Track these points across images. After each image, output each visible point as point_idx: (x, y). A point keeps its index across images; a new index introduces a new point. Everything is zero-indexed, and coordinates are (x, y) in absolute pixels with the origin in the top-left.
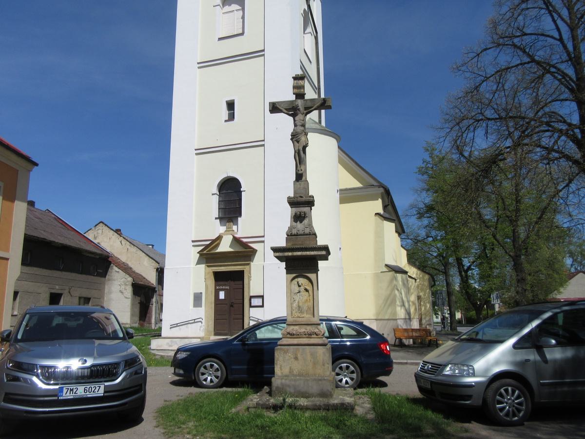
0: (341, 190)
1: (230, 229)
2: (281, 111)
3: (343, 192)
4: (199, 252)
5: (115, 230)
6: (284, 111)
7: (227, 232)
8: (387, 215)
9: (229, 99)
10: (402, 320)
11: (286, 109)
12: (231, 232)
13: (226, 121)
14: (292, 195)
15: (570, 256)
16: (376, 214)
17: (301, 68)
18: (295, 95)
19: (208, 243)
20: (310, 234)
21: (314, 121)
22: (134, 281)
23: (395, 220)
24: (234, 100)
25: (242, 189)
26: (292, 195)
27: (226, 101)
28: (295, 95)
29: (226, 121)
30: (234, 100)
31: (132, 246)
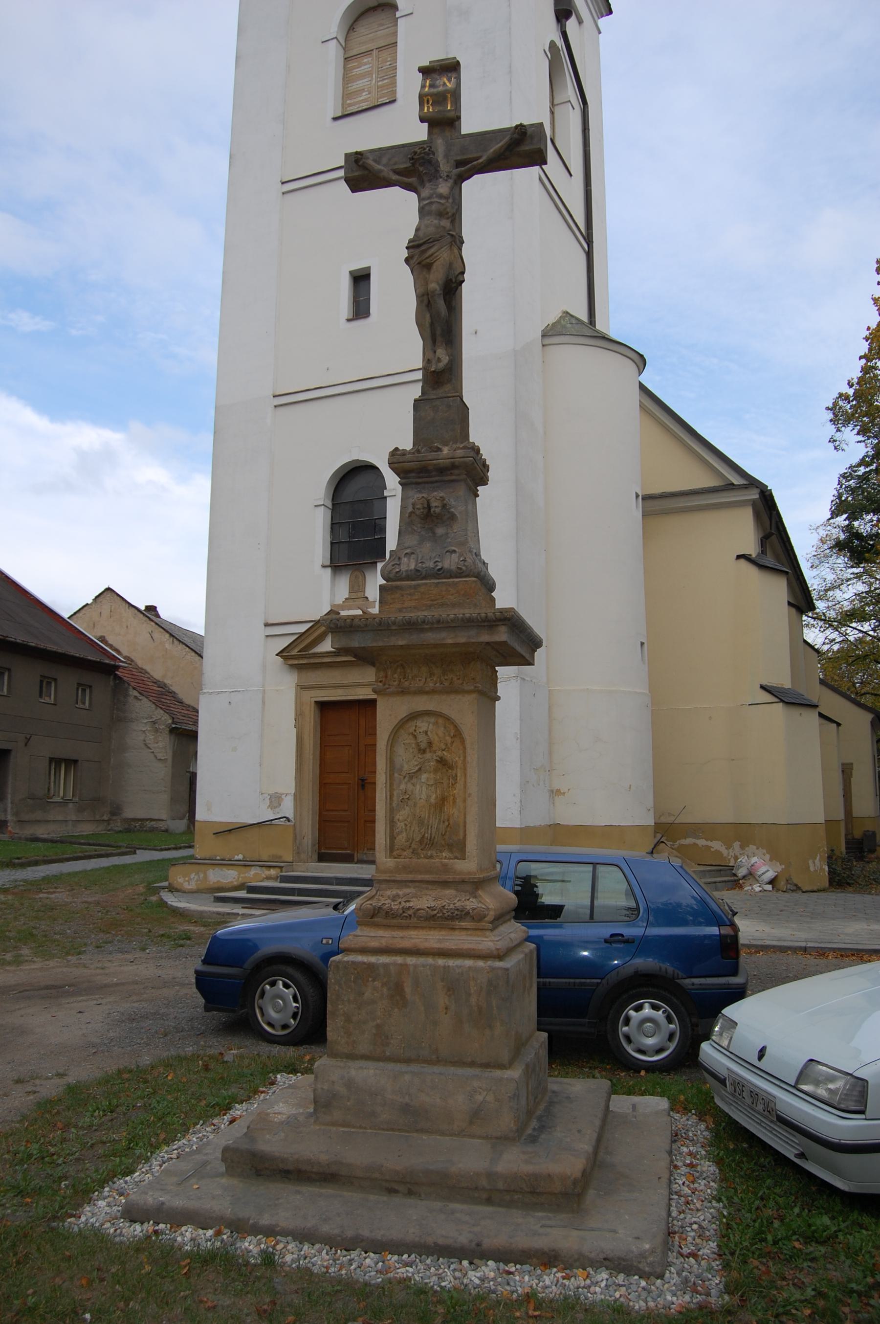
0: (647, 498)
1: (360, 595)
2: (388, 184)
3: (650, 503)
4: (282, 652)
5: (143, 608)
6: (395, 177)
7: (351, 603)
8: (770, 561)
9: (358, 265)
10: (588, 902)
11: (397, 172)
12: (360, 602)
13: (348, 320)
14: (407, 443)
15: (742, 847)
16: (739, 557)
17: (540, 180)
18: (426, 125)
19: (303, 628)
20: (459, 573)
21: (577, 319)
22: (173, 723)
23: (787, 573)
24: (369, 267)
25: (386, 493)
26: (407, 443)
27: (350, 272)
28: (426, 125)
29: (348, 320)
30: (369, 267)
31: (176, 642)
